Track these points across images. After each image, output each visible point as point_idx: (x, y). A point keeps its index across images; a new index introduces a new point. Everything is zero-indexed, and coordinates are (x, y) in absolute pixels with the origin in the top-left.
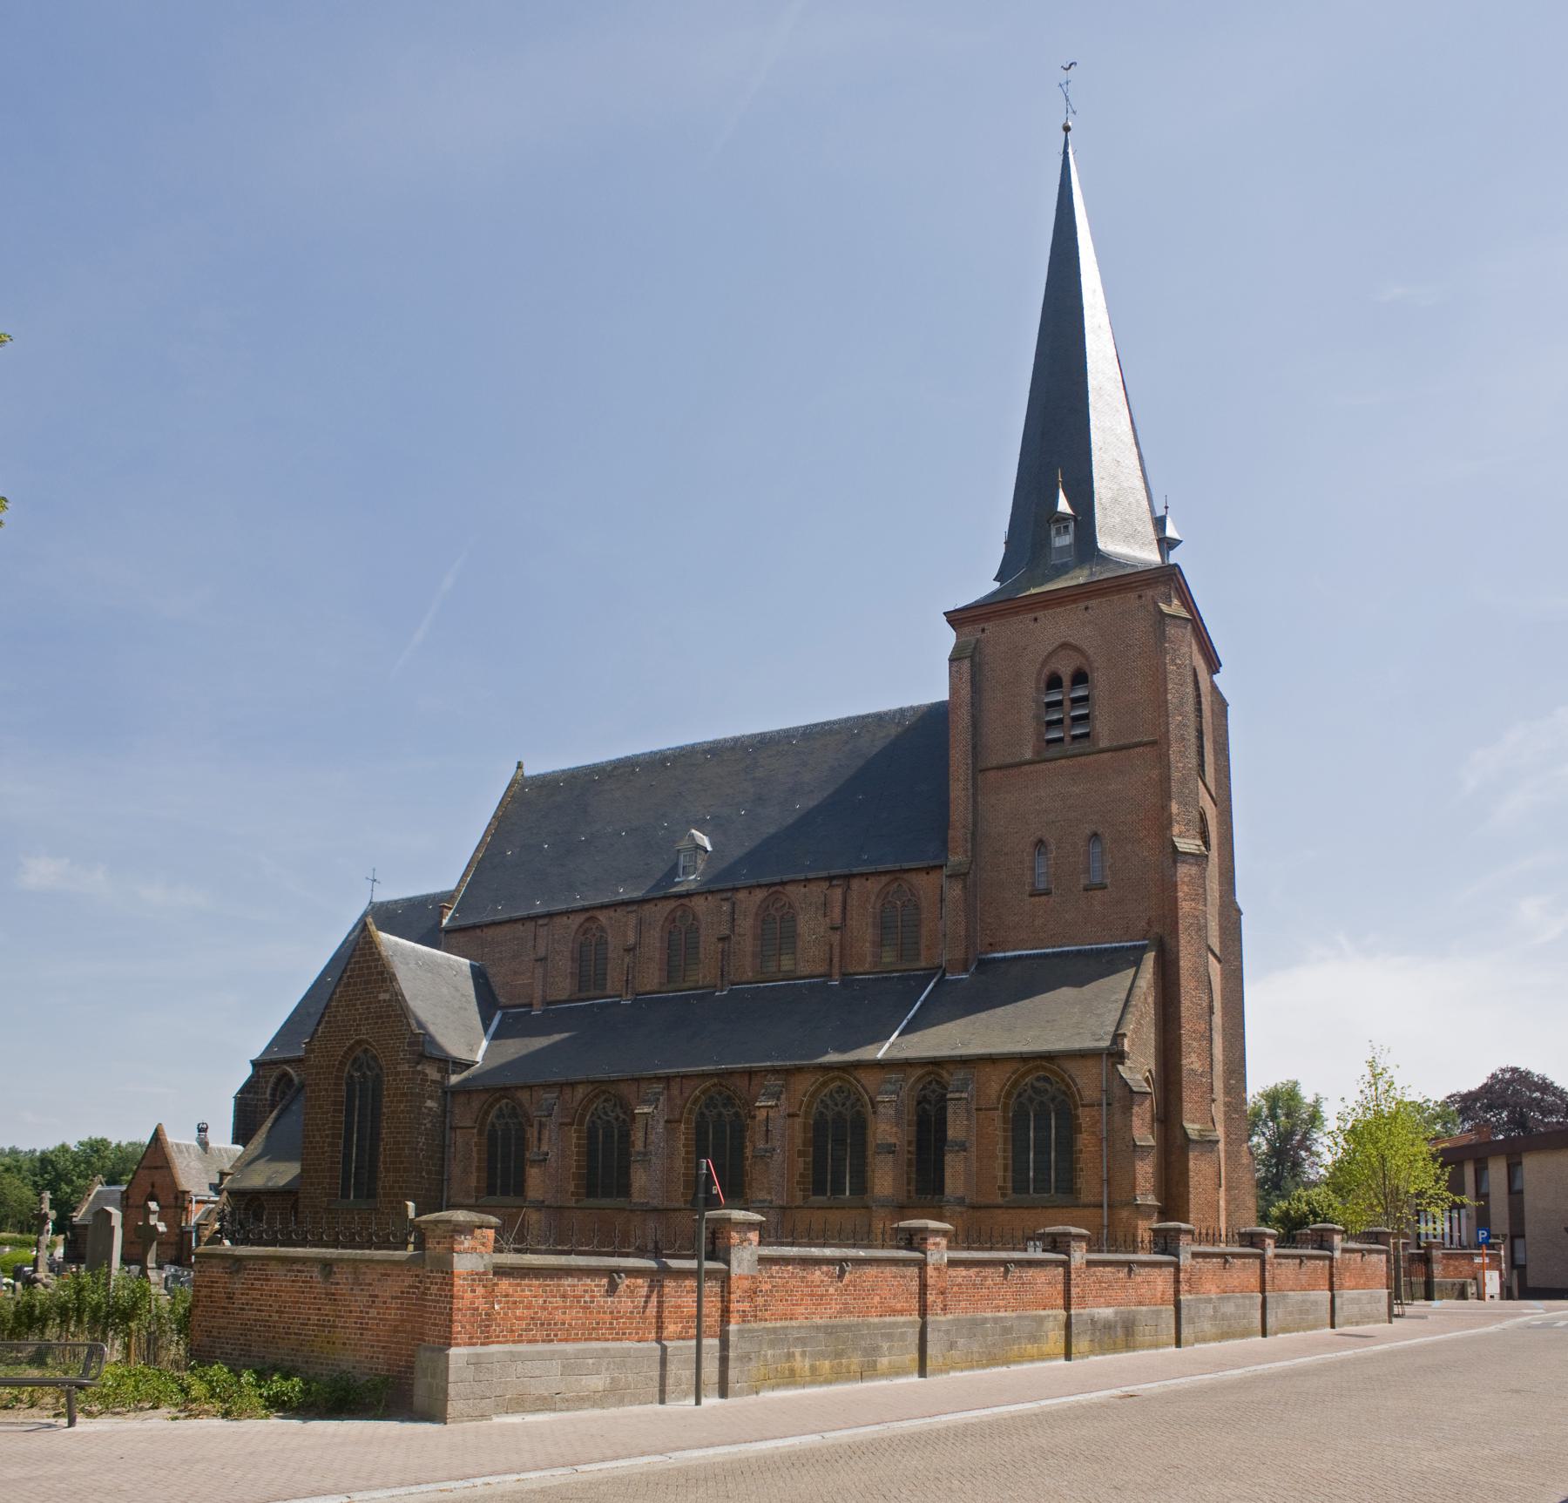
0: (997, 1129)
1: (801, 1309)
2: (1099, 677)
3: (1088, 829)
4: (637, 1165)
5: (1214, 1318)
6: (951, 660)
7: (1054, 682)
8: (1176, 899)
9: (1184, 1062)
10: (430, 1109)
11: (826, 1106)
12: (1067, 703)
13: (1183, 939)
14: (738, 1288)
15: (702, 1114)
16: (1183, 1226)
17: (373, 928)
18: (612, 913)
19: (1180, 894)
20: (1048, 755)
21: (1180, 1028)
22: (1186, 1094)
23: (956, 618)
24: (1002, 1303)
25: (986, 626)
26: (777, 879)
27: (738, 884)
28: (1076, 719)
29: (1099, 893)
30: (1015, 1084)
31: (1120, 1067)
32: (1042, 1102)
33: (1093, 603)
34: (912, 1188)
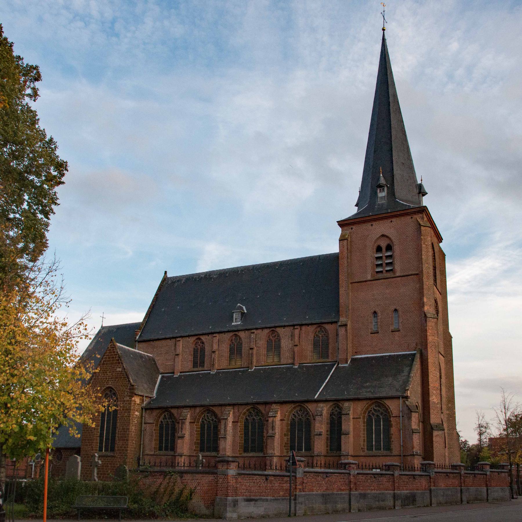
0: (362, 426)
1: (315, 489)
2: (397, 248)
3: (393, 308)
4: (221, 439)
5: (443, 496)
6: (340, 240)
7: (379, 249)
8: (426, 336)
9: (430, 399)
10: (137, 415)
11: (295, 416)
12: (384, 258)
13: (429, 350)
14: (299, 481)
15: (247, 419)
16: (431, 462)
17: (114, 341)
18: (207, 337)
19: (428, 334)
20: (376, 277)
21: (428, 385)
22: (431, 411)
23: (342, 224)
24: (373, 488)
25: (353, 227)
26: (272, 325)
27: (258, 326)
28: (387, 264)
29: (397, 333)
30: (367, 409)
31: (407, 402)
32: (377, 415)
33: (393, 220)
34: (329, 448)
